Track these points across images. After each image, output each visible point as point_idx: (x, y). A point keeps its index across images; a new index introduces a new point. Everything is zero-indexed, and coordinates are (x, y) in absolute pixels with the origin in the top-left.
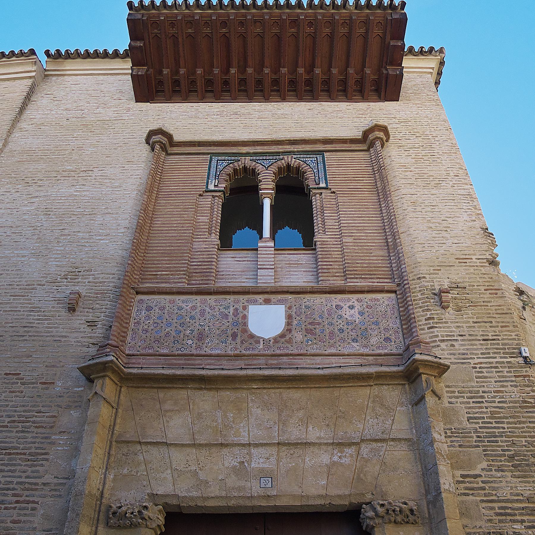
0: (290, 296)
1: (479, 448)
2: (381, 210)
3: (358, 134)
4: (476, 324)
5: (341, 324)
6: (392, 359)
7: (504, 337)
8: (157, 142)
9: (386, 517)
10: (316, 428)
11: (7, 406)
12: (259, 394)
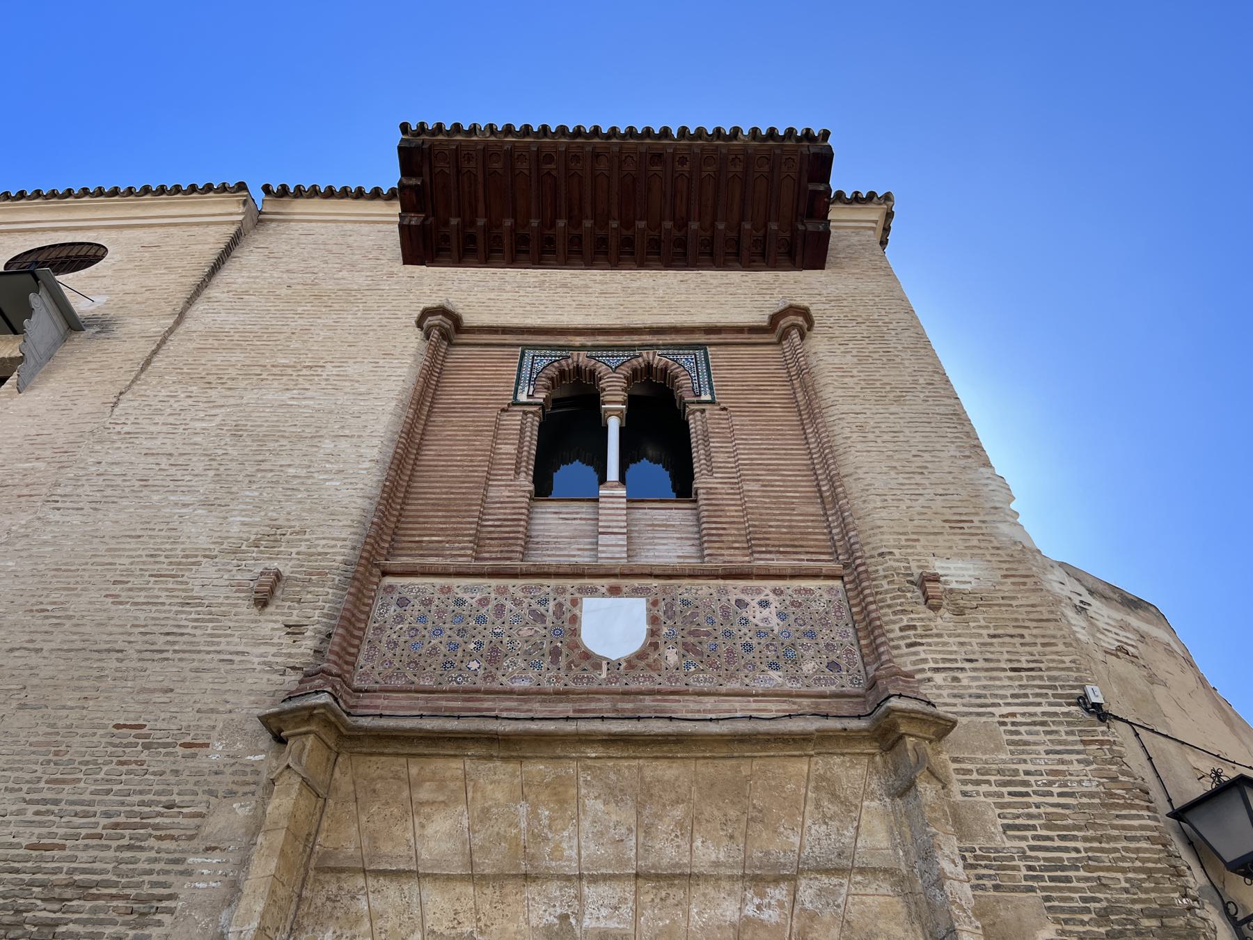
0: (655, 583)
1: (1034, 894)
2: (806, 438)
3: (761, 319)
4: (994, 640)
5: (746, 634)
6: (846, 707)
7: (1051, 665)
10: (709, 843)
11: (108, 792)
12: (599, 768)
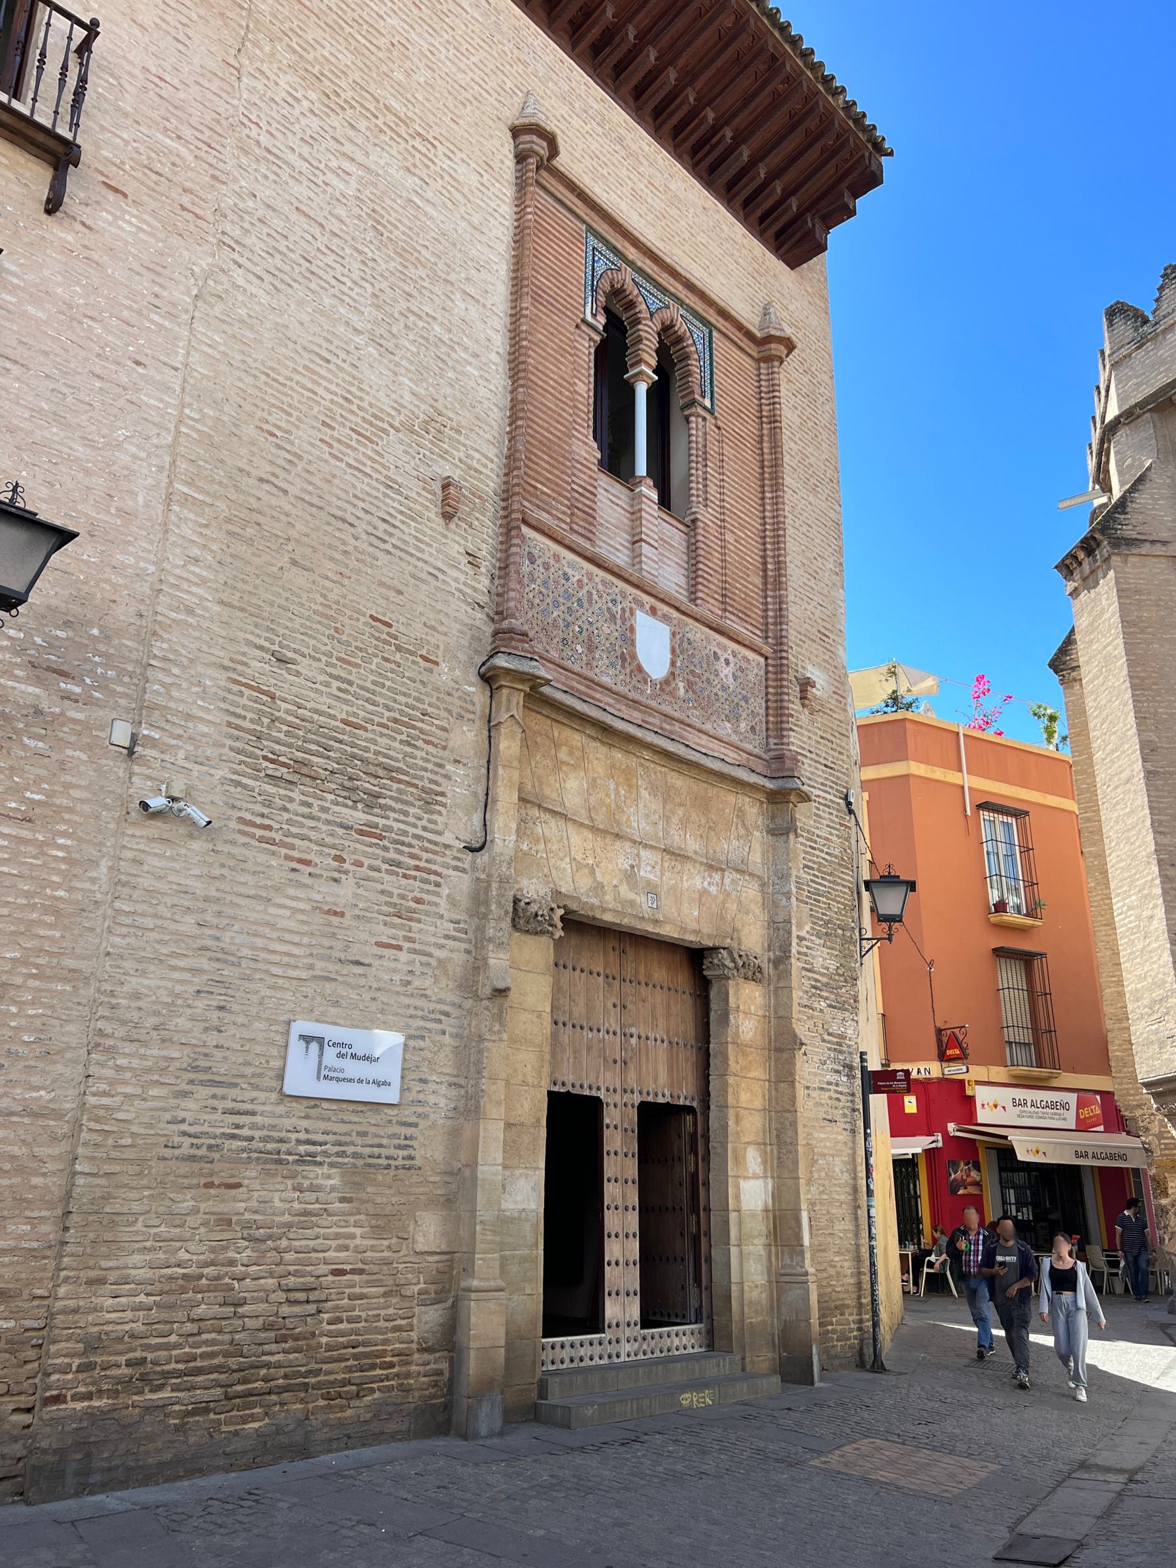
8: (538, 154)
9: (742, 971)
